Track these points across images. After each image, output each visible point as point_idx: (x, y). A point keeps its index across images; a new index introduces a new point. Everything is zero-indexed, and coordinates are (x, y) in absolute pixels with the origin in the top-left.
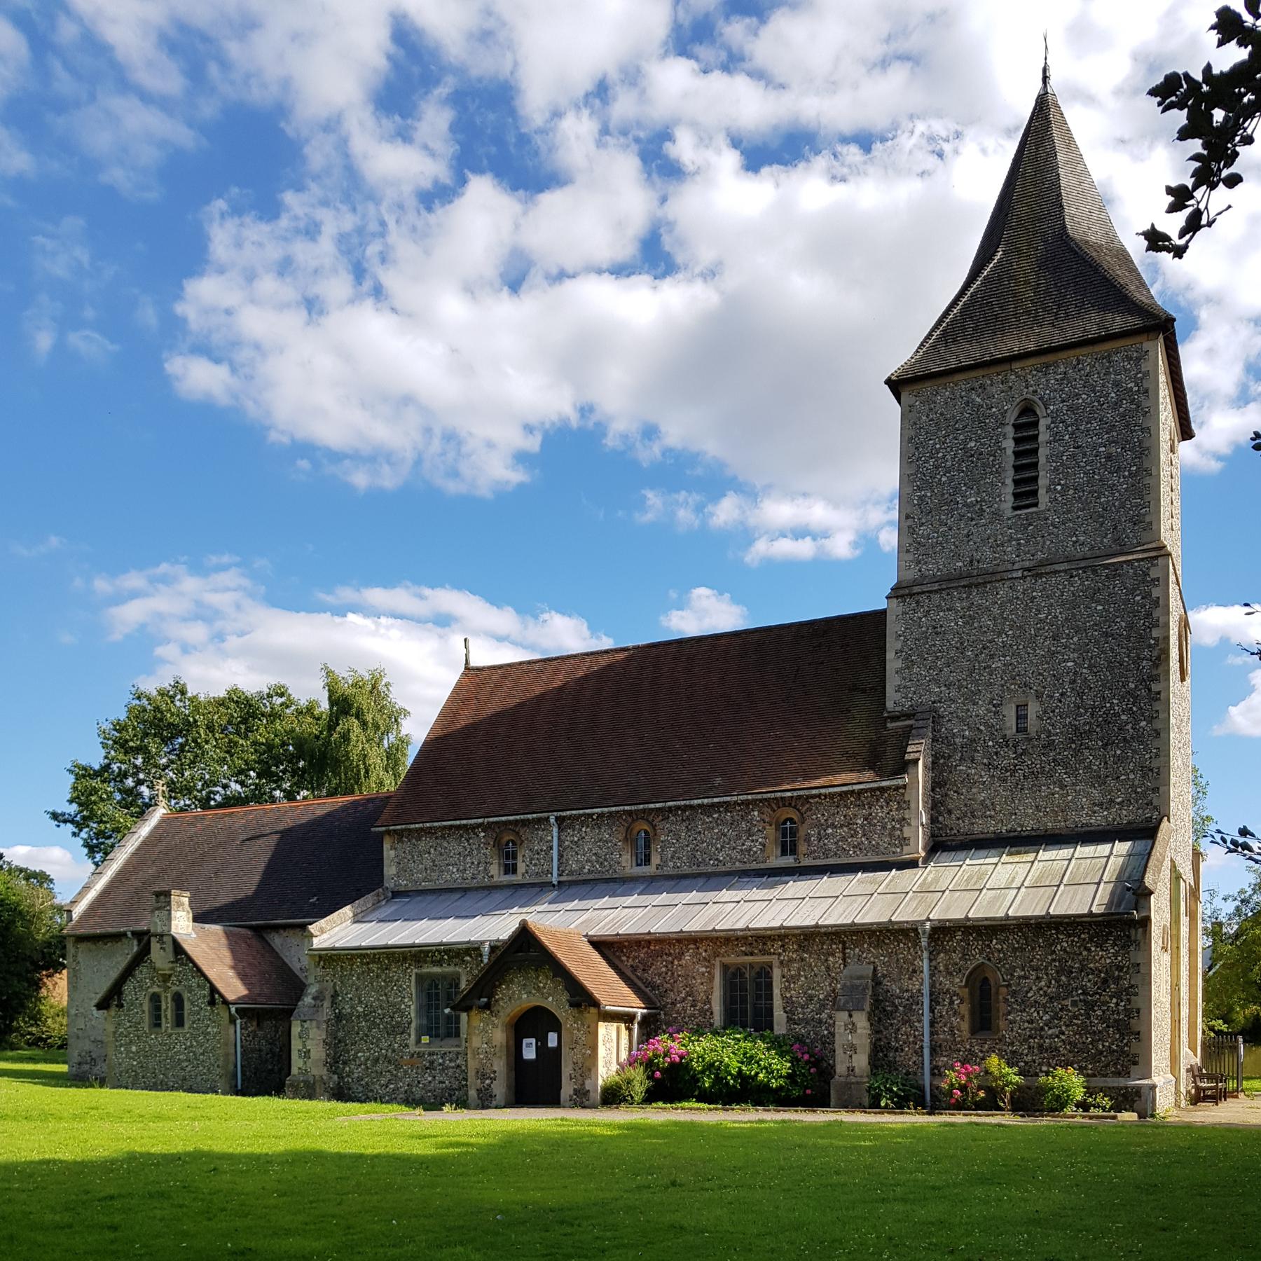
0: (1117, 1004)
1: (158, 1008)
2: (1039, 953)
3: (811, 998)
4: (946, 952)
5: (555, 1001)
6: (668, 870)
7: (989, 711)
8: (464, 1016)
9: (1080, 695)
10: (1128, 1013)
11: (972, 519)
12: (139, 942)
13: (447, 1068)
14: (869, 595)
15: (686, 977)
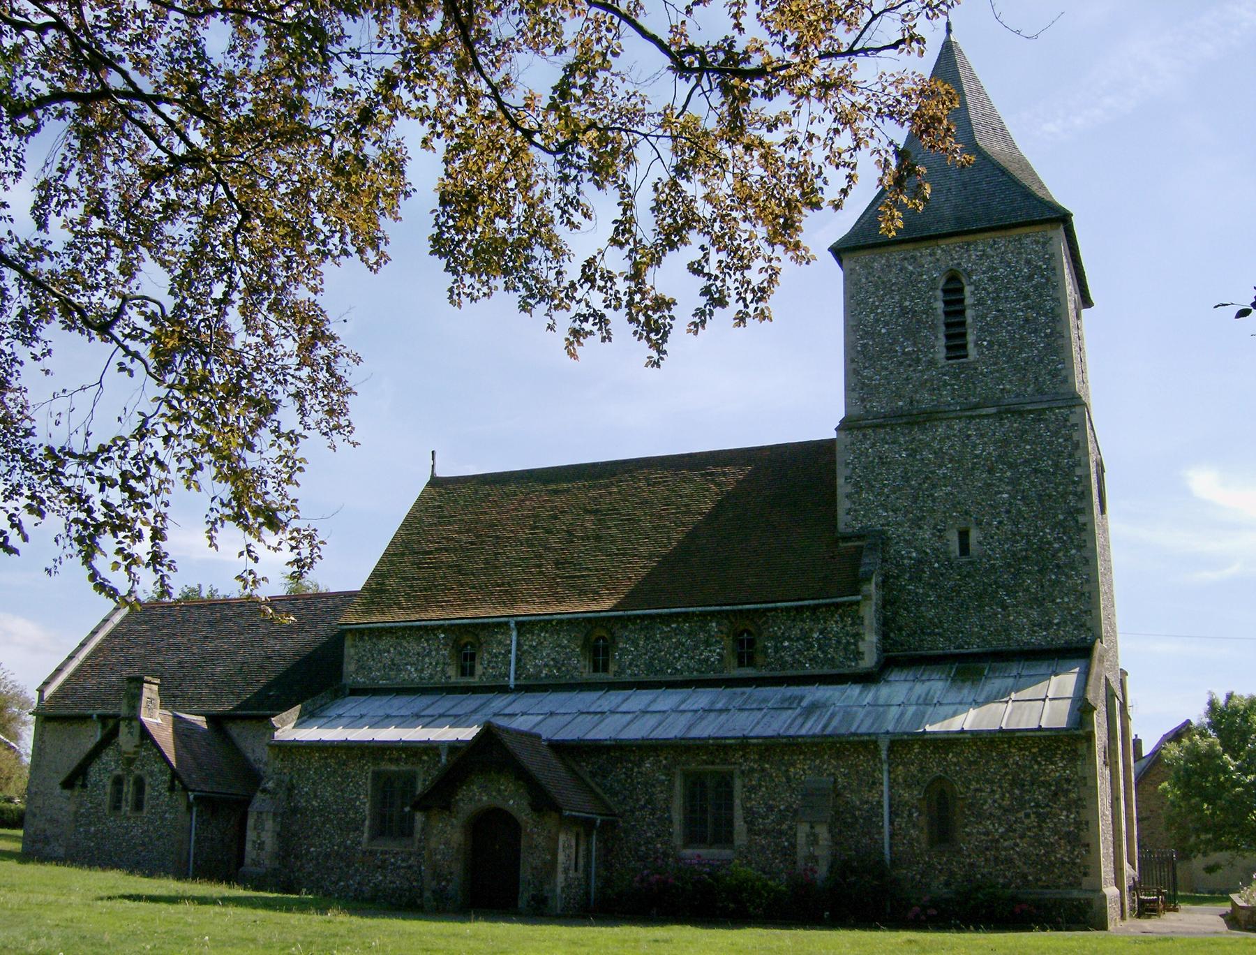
0: (1067, 817)
1: (120, 791)
2: (993, 767)
3: (771, 809)
4: (904, 765)
5: (514, 801)
6: (626, 677)
7: (933, 534)
8: (419, 817)
9: (1016, 524)
10: (1078, 824)
11: (910, 366)
12: (104, 726)
13: (399, 867)
14: (825, 429)
15: (645, 784)
